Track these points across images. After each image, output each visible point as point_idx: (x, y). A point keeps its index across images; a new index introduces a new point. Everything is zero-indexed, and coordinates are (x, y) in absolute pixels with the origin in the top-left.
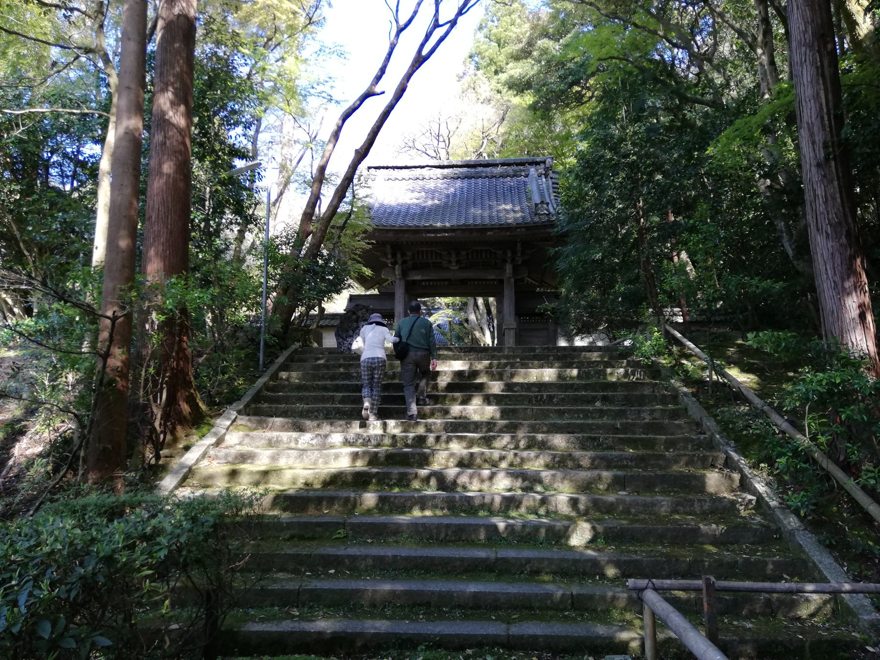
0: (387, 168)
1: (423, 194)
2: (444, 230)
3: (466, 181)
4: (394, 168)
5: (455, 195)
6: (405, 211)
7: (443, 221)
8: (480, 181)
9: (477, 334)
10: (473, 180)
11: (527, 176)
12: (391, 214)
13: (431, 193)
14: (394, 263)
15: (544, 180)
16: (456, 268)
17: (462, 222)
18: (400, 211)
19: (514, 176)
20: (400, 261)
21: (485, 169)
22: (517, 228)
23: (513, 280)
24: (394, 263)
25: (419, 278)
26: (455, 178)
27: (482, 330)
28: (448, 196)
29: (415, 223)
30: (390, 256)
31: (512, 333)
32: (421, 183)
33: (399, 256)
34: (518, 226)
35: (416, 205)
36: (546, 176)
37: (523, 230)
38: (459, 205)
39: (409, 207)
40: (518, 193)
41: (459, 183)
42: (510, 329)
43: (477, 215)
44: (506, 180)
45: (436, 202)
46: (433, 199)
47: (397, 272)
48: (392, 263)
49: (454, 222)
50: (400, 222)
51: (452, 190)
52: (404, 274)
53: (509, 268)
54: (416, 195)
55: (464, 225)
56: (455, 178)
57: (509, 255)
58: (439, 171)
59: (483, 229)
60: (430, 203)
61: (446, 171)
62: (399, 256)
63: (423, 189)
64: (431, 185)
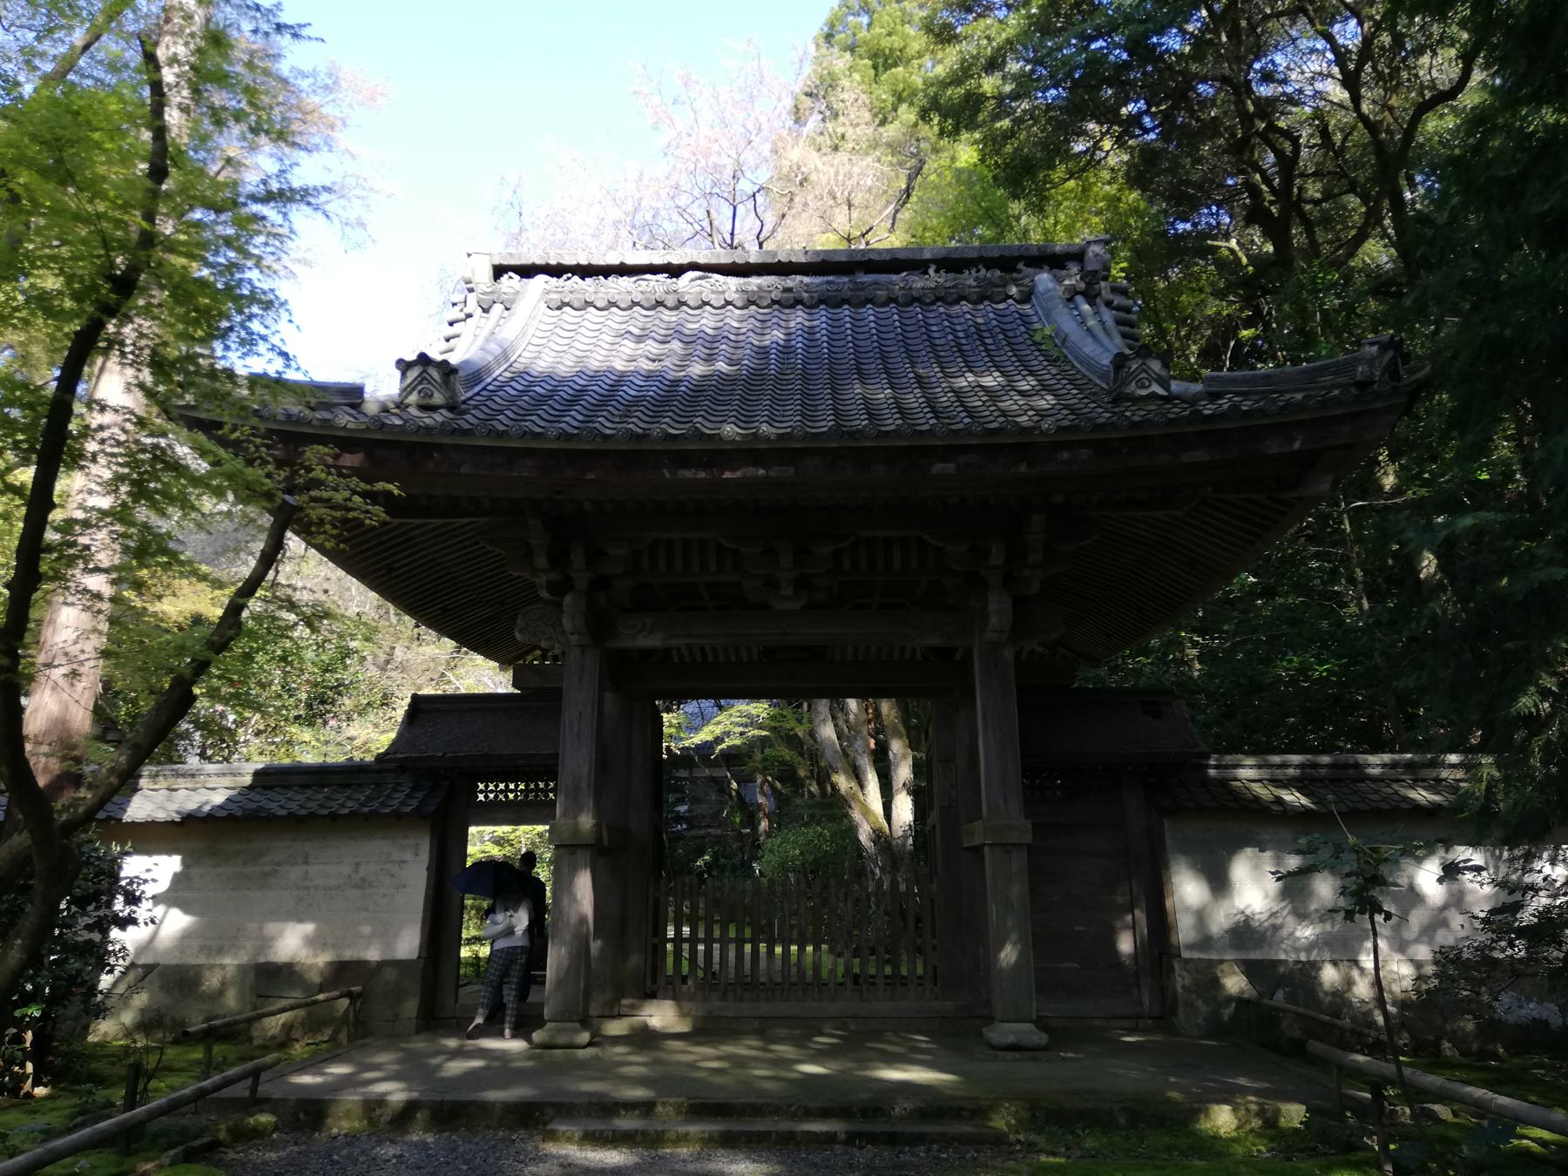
0: (556, 271)
1: (676, 345)
2: (750, 452)
3: (822, 313)
4: (586, 271)
5: (786, 350)
6: (604, 392)
7: (746, 419)
8: (869, 312)
9: (843, 782)
10: (846, 311)
11: (1026, 298)
12: (541, 400)
13: (710, 345)
14: (561, 588)
15: (1086, 307)
16: (796, 605)
17: (825, 424)
18: (583, 391)
19: (981, 298)
20: (582, 581)
21: (883, 278)
22: (1059, 446)
23: (1008, 654)
24: (561, 588)
25: (653, 641)
26: (789, 302)
27: (857, 776)
28: (763, 352)
29: (635, 425)
30: (541, 561)
31: (1018, 862)
32: (668, 316)
33: (578, 558)
34: (1065, 439)
35: (649, 376)
36: (1091, 297)
37: (1084, 454)
38: (806, 377)
39: (621, 379)
40: (1013, 345)
41: (798, 318)
42: (1007, 847)
43: (874, 398)
44: (956, 309)
45: (722, 366)
46: (710, 359)
47: (567, 624)
48: (551, 586)
49: (790, 422)
50: (572, 421)
51: (778, 335)
52: (598, 626)
53: (998, 610)
54: (652, 347)
55: (838, 432)
56: (789, 302)
57: (997, 556)
58: (733, 282)
59: (910, 453)
60: (697, 369)
61: (755, 282)
62: (578, 558)
63: (677, 333)
64: (707, 322)
